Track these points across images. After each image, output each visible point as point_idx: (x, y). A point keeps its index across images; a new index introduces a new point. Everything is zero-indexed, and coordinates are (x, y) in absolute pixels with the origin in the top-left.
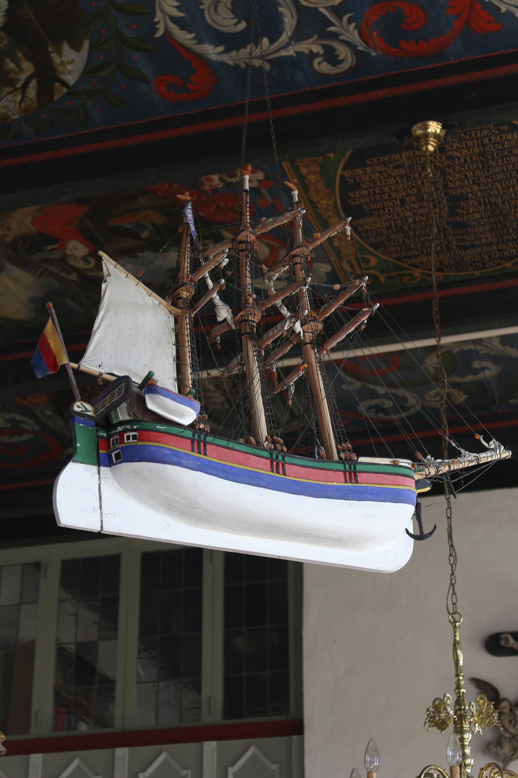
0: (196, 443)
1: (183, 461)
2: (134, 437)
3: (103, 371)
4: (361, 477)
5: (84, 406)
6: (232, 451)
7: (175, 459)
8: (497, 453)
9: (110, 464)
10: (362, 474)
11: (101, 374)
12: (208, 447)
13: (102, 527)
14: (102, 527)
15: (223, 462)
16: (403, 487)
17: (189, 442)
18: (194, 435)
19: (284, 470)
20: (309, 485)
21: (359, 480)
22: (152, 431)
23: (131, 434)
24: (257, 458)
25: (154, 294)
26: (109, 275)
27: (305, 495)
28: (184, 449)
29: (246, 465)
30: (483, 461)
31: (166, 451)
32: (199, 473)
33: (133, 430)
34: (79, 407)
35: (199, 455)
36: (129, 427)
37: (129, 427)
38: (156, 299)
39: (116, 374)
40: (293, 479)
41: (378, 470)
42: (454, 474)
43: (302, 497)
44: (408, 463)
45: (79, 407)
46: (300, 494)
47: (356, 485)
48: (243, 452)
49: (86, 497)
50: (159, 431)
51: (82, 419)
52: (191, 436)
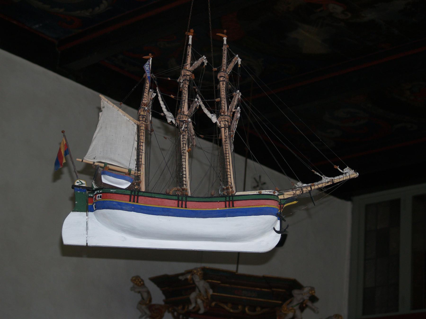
0: (132, 197)
1: (124, 207)
2: (101, 196)
3: (95, 161)
4: (236, 203)
5: (81, 182)
6: (154, 199)
7: (119, 207)
8: (349, 174)
9: (92, 211)
10: (237, 202)
11: (94, 163)
12: (139, 198)
13: (87, 244)
14: (87, 244)
15: (147, 205)
16: (263, 206)
17: (128, 197)
18: (131, 193)
19: (186, 205)
20: (201, 212)
21: (235, 205)
22: (108, 193)
23: (99, 195)
24: (169, 200)
25: (127, 114)
26: (104, 107)
27: (197, 217)
28: (125, 200)
29: (162, 205)
30: (335, 181)
31: (114, 203)
32: (133, 212)
33: (100, 193)
34: (78, 182)
35: (133, 203)
36: (98, 191)
37: (98, 191)
38: (127, 117)
39: (103, 161)
40: (192, 209)
41: (242, 199)
42: (320, 189)
43: (195, 219)
44: (270, 192)
45: (78, 182)
46: (194, 217)
47: (233, 208)
48: (160, 198)
49: (81, 229)
50: (112, 193)
51: (78, 189)
52: (130, 194)
